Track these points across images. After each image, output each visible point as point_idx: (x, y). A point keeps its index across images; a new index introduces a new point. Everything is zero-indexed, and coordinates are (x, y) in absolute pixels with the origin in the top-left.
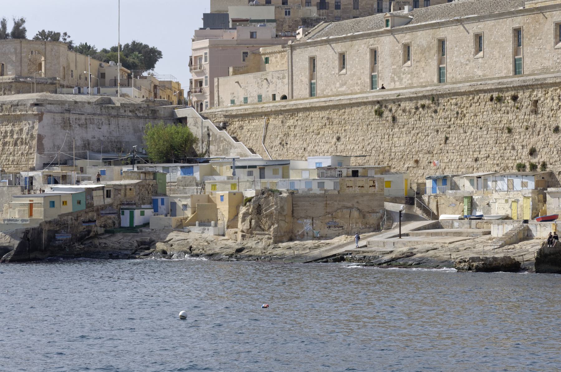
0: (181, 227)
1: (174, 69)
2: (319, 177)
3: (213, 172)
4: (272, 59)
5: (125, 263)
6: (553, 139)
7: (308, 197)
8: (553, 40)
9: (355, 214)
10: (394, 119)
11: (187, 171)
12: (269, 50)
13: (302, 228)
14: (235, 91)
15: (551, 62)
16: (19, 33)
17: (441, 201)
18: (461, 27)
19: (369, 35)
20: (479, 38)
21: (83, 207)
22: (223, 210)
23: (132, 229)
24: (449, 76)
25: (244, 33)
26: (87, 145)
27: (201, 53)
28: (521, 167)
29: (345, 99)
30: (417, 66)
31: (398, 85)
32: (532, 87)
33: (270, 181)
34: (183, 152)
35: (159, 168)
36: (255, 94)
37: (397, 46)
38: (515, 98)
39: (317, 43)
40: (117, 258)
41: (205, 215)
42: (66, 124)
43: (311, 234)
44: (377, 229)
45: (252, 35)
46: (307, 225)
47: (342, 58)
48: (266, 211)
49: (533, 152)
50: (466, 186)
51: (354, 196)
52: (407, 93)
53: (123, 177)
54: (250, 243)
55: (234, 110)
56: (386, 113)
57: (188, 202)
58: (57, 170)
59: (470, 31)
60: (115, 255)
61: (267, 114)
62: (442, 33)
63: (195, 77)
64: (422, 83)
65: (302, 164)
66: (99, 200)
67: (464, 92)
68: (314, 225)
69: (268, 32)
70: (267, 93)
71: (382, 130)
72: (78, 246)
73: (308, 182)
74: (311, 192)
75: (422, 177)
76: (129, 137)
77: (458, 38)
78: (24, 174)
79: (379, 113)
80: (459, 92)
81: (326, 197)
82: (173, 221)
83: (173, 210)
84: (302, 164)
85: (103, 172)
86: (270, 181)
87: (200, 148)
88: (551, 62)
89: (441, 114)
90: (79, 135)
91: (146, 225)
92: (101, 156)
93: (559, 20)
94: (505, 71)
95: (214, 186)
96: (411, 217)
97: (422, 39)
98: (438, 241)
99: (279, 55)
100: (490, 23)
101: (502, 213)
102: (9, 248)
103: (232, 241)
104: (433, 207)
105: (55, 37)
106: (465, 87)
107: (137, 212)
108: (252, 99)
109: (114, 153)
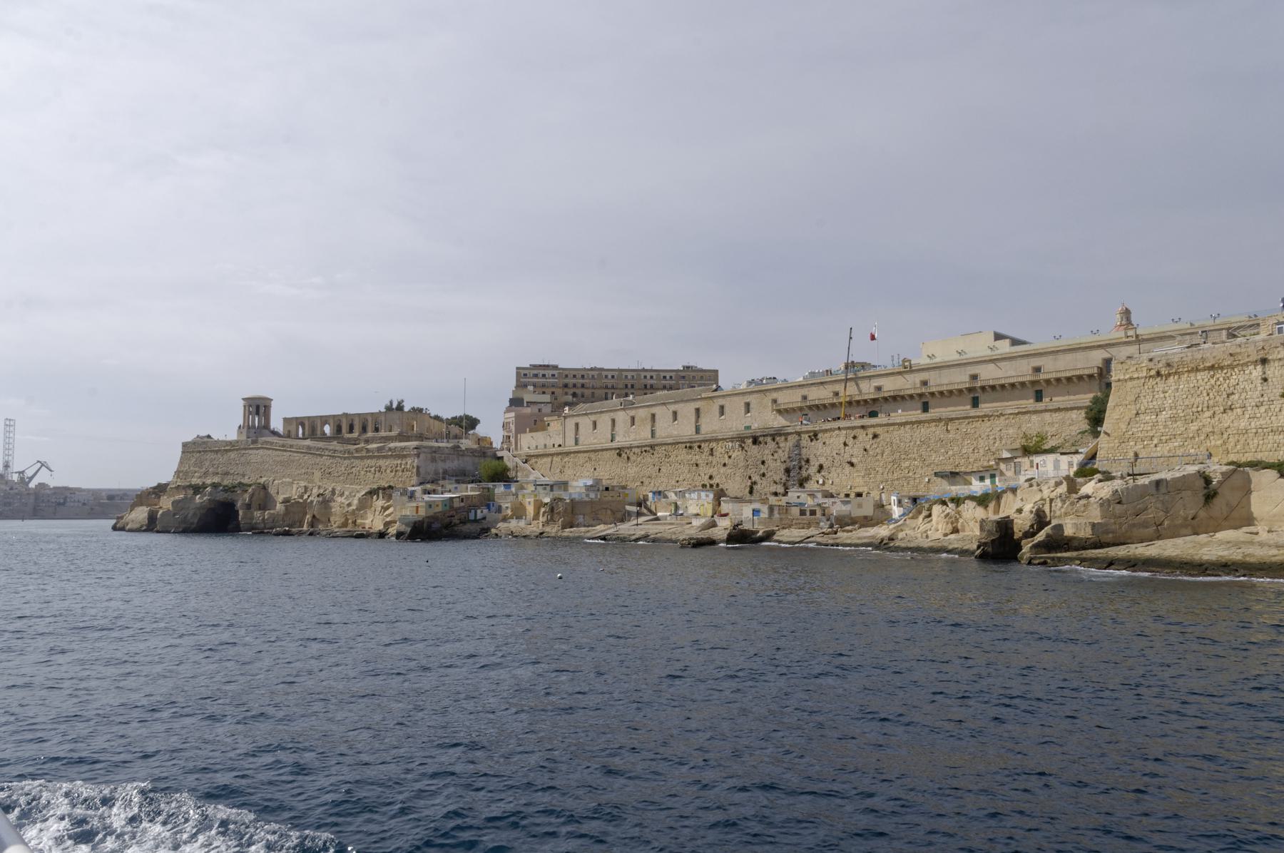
0: (505, 519)
1: (492, 428)
3: (522, 488)
5: (470, 542)
6: (723, 470)
11: (507, 487)
14: (529, 442)
16: (400, 408)
20: (675, 413)
22: (530, 510)
23: (476, 521)
24: (657, 434)
25: (535, 409)
26: (445, 472)
28: (704, 486)
29: (599, 447)
32: (709, 441)
33: (558, 493)
34: (501, 476)
35: (490, 485)
41: (519, 513)
42: (434, 460)
44: (622, 521)
46: (581, 519)
47: (595, 423)
49: (711, 477)
50: (672, 496)
52: (636, 443)
53: (470, 490)
54: (547, 529)
55: (532, 452)
58: (429, 486)
61: (552, 455)
62: (654, 410)
65: (575, 484)
66: (457, 504)
69: (547, 409)
70: (550, 443)
72: (445, 532)
73: (580, 494)
75: (647, 491)
76: (470, 467)
77: (663, 413)
78: (411, 489)
79: (619, 455)
81: (592, 502)
82: (500, 516)
83: (499, 510)
84: (575, 484)
86: (558, 493)
87: (511, 474)
90: (441, 466)
91: (484, 518)
96: (639, 514)
97: (642, 414)
98: (661, 528)
100: (682, 405)
103: (536, 528)
104: (653, 508)
105: (420, 410)
106: (670, 440)
108: (541, 446)
109: (462, 476)
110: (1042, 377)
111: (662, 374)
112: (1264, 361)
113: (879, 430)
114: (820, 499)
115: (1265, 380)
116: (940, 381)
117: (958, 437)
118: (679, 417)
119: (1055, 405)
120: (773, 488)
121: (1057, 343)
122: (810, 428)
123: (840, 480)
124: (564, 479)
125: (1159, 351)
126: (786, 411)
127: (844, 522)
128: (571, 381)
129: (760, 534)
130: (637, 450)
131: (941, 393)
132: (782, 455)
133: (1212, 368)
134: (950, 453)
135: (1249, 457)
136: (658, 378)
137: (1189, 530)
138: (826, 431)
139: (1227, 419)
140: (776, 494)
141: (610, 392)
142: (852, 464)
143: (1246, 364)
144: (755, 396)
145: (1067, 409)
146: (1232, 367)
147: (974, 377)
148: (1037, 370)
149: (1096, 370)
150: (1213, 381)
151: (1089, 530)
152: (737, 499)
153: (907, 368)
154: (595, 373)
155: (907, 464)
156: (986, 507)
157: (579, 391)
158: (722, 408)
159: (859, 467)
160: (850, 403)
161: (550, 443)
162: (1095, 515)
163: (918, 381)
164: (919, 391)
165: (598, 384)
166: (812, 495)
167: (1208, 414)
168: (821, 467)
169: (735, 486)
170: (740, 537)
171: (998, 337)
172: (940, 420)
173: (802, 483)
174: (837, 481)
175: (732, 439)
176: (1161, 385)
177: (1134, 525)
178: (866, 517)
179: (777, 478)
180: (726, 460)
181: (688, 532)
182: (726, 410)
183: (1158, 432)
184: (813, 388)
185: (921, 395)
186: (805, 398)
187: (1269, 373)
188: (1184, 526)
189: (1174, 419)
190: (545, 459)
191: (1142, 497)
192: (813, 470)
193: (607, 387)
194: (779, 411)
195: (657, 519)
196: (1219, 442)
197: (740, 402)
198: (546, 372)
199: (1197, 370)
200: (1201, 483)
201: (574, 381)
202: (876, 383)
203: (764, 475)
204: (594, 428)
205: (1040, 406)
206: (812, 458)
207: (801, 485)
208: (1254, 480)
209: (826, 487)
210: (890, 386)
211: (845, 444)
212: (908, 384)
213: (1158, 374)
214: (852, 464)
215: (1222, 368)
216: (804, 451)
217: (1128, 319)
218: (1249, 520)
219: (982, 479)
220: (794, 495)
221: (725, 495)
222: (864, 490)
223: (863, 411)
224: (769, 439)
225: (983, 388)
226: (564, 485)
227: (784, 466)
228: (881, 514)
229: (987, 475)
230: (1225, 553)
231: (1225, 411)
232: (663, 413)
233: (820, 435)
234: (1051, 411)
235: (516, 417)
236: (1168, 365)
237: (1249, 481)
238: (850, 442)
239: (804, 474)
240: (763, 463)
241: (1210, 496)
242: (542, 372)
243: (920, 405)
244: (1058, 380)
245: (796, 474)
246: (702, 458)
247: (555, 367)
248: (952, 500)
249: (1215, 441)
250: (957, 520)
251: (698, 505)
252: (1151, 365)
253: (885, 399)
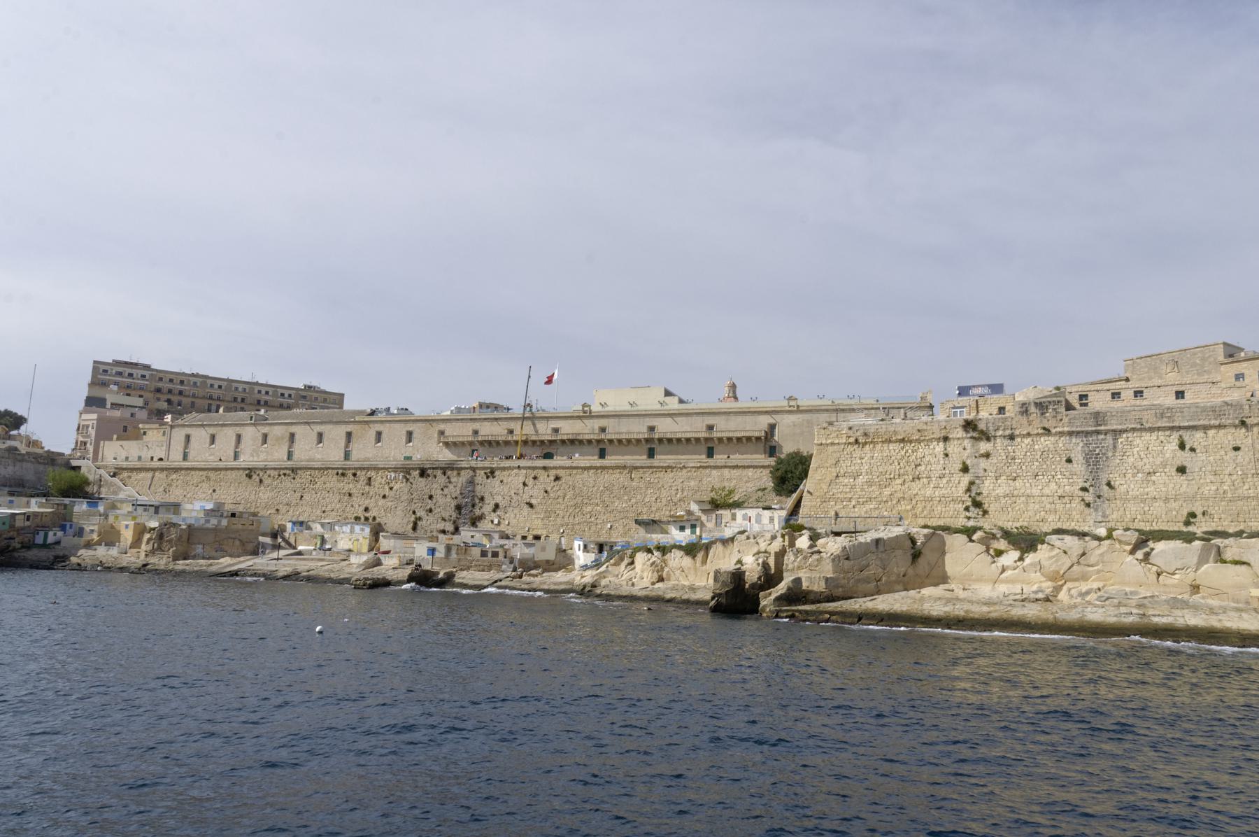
0: (88, 545)
3: (114, 507)
4: (149, 433)
6: (381, 502)
9: (237, 543)
10: (261, 481)
12: (147, 426)
14: (115, 452)
17: (299, 537)
19: (236, 425)
20: (320, 435)
21: (6, 527)
22: (127, 535)
23: (44, 545)
24: (295, 457)
27: (90, 423)
28: (357, 518)
32: (368, 469)
34: (77, 489)
35: (67, 501)
36: (136, 455)
38: (355, 475)
40: (37, 568)
44: (255, 553)
45: (132, 415)
49: (366, 509)
50: (317, 528)
51: (237, 531)
52: (272, 464)
55: (125, 464)
56: (255, 477)
57: (96, 528)
60: (36, 566)
61: (154, 470)
62: (293, 429)
63: (81, 439)
65: (188, 506)
66: (20, 523)
71: (250, 488)
73: (197, 519)
79: (249, 476)
81: (216, 530)
83: (80, 532)
84: (188, 506)
85: (1187, 523)
89: (298, 480)
91: (58, 543)
92: (7, 489)
95: (117, 517)
96: (279, 547)
97: (277, 431)
100: (330, 427)
101: (347, 547)
103: (136, 558)
104: (292, 541)
107: (51, 534)
110: (716, 435)
111: (280, 391)
112: (946, 439)
113: (561, 473)
114: (497, 541)
115: (947, 455)
116: (617, 430)
117: (641, 485)
118: (325, 439)
119: (734, 463)
120: (441, 526)
121: (819, 402)
122: (487, 464)
123: (518, 520)
124: (171, 498)
125: (857, 420)
126: (455, 444)
127: (527, 566)
128: (166, 386)
129: (441, 575)
130: (272, 473)
131: (620, 441)
132: (454, 490)
133: (902, 440)
134: (633, 500)
135: (941, 523)
136: (275, 393)
137: (900, 587)
138: (504, 469)
139: (915, 487)
140: (444, 532)
141: (214, 404)
142: (531, 506)
143: (931, 440)
144: (419, 425)
145: (744, 467)
146: (919, 441)
147: (652, 429)
148: (710, 428)
149: (763, 434)
150: (903, 453)
151: (823, 584)
152: (396, 535)
153: (587, 414)
154: (198, 380)
155: (589, 508)
156: (694, 557)
157: (175, 399)
158: (379, 434)
159: (538, 509)
160: (525, 442)
161: (146, 455)
162: (828, 570)
163: (596, 427)
164: (597, 437)
165: (200, 392)
166: (488, 535)
167: (899, 481)
168: (497, 506)
169: (395, 520)
170: (423, 578)
171: (668, 393)
172: (625, 467)
173: (474, 522)
174: (513, 522)
175: (395, 469)
176: (858, 452)
177: (859, 581)
178: (548, 561)
179: (446, 515)
180: (387, 492)
181: (347, 570)
182: (384, 436)
183: (859, 496)
184: (486, 423)
185: (599, 441)
186: (476, 432)
187: (950, 450)
188: (898, 582)
189: (870, 483)
190: (143, 475)
191: (865, 554)
192: (487, 508)
193: (211, 398)
194: (447, 444)
195: (300, 553)
196: (909, 507)
197: (401, 430)
198: (133, 371)
199: (890, 441)
200: (909, 543)
201: (171, 386)
202: (554, 424)
203: (431, 511)
204: (208, 442)
205: (711, 462)
206: (487, 495)
207: (474, 524)
208: (948, 543)
209: (502, 528)
210: (568, 429)
211: (524, 484)
212: (587, 429)
213: (857, 441)
214: (531, 506)
215: (911, 442)
216: (478, 488)
217: (734, 392)
218: (943, 579)
219: (682, 528)
220: (466, 534)
221: (383, 531)
222: (543, 532)
223: (538, 451)
224: (439, 473)
225: (660, 440)
226: (176, 507)
227: (454, 503)
228: (563, 560)
229: (688, 525)
230: (947, 609)
231: (913, 480)
232: (305, 435)
233: (497, 473)
234: (730, 467)
235: (98, 420)
236: (865, 434)
237: (944, 544)
238: (530, 482)
239: (478, 512)
240: (431, 497)
241: (916, 556)
242: (128, 371)
243: (597, 451)
244: (730, 439)
245: (468, 511)
246: (357, 487)
247: (147, 367)
248: (658, 548)
249: (905, 506)
250: (662, 569)
251: (351, 539)
252: (850, 433)
253: (563, 442)
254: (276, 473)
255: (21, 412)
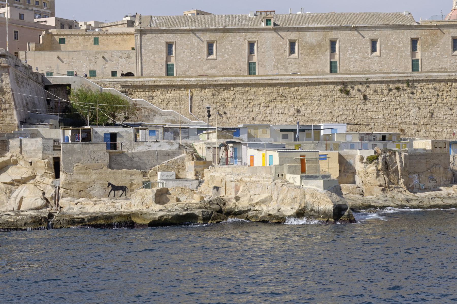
2: (360, 140)
7: (415, 155)
8: (369, 51)
10: (365, 97)
13: (412, 181)
15: (448, 64)
18: (356, 33)
30: (305, 59)
31: (282, 72)
37: (281, 42)
39: (179, 31)
43: (418, 186)
48: (392, 167)
56: (353, 92)
59: (366, 36)
64: (311, 72)
67: (443, 80)
68: (420, 179)
74: (417, 151)
80: (438, 80)
88: (448, 64)
93: (456, 35)
94: (403, 68)
99: (80, 38)
102: (343, 207)
130: (379, 87)
254: (384, 87)
255: (66, 43)
